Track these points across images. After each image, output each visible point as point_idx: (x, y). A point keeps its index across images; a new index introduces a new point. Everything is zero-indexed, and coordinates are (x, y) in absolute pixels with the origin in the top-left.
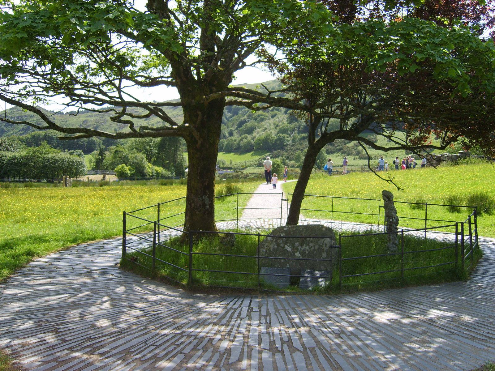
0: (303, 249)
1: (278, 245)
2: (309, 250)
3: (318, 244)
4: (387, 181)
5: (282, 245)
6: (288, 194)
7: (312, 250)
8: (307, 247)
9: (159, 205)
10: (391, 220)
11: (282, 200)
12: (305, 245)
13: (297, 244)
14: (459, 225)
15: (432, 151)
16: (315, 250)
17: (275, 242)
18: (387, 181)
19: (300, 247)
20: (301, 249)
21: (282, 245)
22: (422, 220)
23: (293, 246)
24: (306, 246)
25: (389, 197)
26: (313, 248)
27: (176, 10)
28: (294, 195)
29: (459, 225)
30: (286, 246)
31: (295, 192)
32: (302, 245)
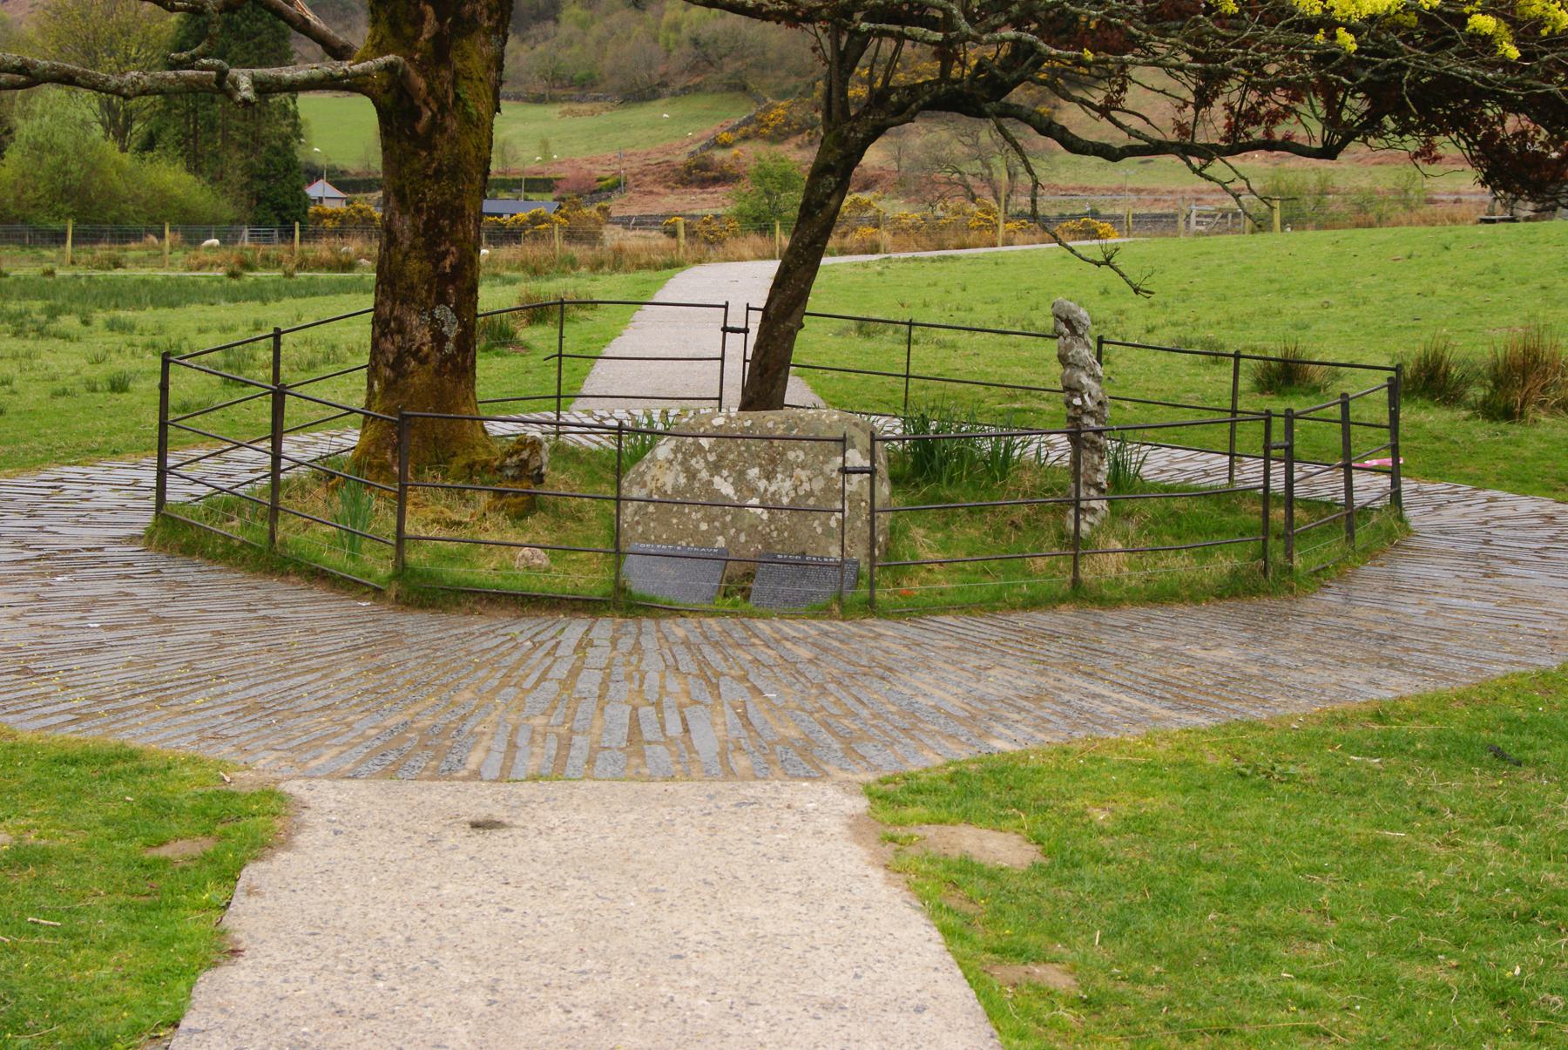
0: (772, 489)
1: (692, 475)
2: (792, 494)
3: (822, 473)
4: (1099, 264)
5: (704, 475)
6: (748, 309)
7: (801, 493)
8: (788, 484)
9: (277, 334)
10: (1077, 401)
11: (725, 330)
12: (779, 476)
13: (753, 472)
14: (1278, 424)
15: (661, 284)
16: (810, 494)
17: (682, 464)
18: (1099, 264)
19: (762, 484)
20: (766, 490)
21: (704, 475)
22: (556, 343)
23: (740, 480)
24: (783, 480)
25: (1075, 323)
26: (806, 486)
27: (468, 551)
28: (765, 311)
29: (1278, 424)
30: (717, 479)
31: (770, 300)
32: (769, 476)
